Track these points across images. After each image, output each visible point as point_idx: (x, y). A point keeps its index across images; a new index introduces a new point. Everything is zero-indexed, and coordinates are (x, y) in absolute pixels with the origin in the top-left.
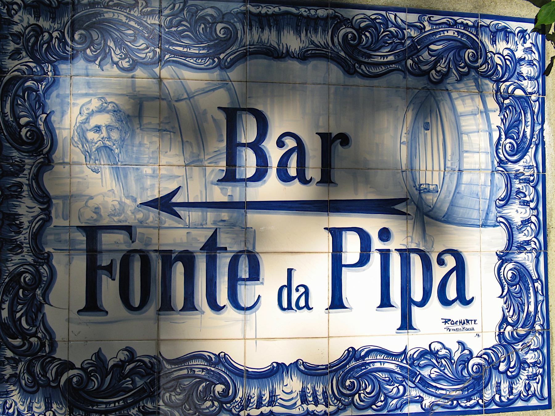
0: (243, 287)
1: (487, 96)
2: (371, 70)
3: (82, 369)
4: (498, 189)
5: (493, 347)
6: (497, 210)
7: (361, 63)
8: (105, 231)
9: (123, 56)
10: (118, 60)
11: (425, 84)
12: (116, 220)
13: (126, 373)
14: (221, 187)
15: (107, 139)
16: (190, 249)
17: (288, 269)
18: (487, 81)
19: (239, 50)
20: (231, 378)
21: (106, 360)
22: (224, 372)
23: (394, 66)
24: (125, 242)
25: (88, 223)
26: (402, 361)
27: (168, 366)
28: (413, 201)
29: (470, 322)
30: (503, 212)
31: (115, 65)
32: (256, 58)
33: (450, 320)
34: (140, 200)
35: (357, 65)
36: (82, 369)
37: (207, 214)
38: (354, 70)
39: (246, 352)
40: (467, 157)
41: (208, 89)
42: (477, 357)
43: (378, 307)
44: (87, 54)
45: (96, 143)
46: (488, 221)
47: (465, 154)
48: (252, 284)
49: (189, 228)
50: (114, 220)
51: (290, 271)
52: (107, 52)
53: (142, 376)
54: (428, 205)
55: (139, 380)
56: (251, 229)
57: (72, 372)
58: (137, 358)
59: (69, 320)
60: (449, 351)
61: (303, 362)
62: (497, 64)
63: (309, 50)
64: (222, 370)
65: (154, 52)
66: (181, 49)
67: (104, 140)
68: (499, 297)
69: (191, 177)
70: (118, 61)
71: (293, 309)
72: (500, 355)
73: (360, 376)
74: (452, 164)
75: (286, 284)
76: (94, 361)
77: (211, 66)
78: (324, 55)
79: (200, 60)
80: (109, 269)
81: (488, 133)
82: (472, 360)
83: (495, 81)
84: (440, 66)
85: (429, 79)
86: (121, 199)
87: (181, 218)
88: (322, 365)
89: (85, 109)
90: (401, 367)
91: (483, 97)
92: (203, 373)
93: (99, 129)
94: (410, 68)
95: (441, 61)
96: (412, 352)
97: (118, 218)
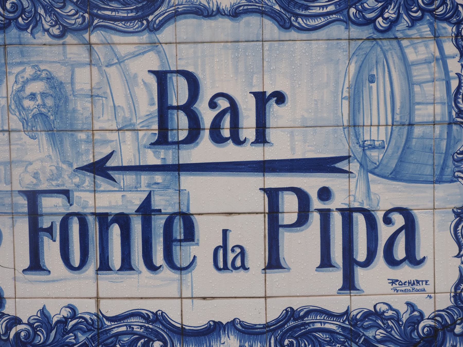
0: (178, 248)
1: (445, 41)
2: (308, 23)
3: (29, 324)
4: (456, 141)
5: (448, 308)
6: (454, 164)
7: (297, 16)
8: (45, 195)
9: (54, 23)
10: (49, 27)
11: (371, 34)
12: (54, 185)
13: (69, 329)
14: (154, 150)
15: (42, 107)
16: (126, 211)
17: (223, 230)
18: (445, 25)
19: (168, 10)
20: (168, 335)
21: (50, 316)
22: (162, 329)
23: (334, 16)
24: (64, 206)
25: (29, 188)
26: (344, 322)
27: (108, 323)
28: (356, 158)
29: (421, 283)
30: (461, 167)
31: (46, 33)
32: (185, 18)
33: (397, 281)
34: (76, 165)
35: (293, 18)
36: (29, 324)
37: (141, 177)
38: (290, 24)
39: (183, 310)
40: (419, 109)
41: (138, 53)
42: (428, 319)
43: (318, 267)
44: (18, 22)
45: (32, 110)
46: (444, 177)
47: (417, 107)
48: (187, 245)
49: (124, 191)
50: (52, 184)
51: (225, 232)
52: (38, 19)
53: (84, 332)
54: (372, 162)
55: (81, 335)
56: (185, 191)
57: (19, 327)
58: (79, 315)
59: (15, 279)
60: (397, 312)
61: (240, 321)
62: (458, 4)
63: (240, 6)
64: (160, 328)
65: (84, 18)
66: (108, 13)
67: (40, 108)
68: (455, 257)
69: (124, 142)
70: (49, 29)
71: (229, 269)
72: (455, 317)
73: (299, 336)
74: (401, 117)
75: (222, 245)
76: (39, 317)
77: (140, 29)
78: (257, 10)
79: (129, 24)
80: (50, 231)
81: (444, 82)
82: (422, 322)
83: (455, 24)
84: (388, 12)
85: (376, 28)
86: (58, 164)
87: (116, 182)
88: (260, 325)
89: (20, 77)
90: (343, 328)
91: (439, 42)
92: (142, 330)
93: (34, 97)
94: (353, 18)
95: (390, 6)
96: (355, 313)
97: (56, 182)
